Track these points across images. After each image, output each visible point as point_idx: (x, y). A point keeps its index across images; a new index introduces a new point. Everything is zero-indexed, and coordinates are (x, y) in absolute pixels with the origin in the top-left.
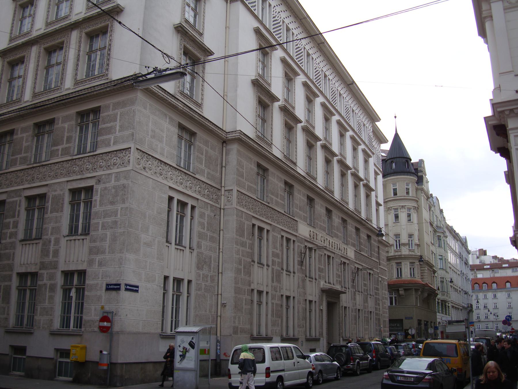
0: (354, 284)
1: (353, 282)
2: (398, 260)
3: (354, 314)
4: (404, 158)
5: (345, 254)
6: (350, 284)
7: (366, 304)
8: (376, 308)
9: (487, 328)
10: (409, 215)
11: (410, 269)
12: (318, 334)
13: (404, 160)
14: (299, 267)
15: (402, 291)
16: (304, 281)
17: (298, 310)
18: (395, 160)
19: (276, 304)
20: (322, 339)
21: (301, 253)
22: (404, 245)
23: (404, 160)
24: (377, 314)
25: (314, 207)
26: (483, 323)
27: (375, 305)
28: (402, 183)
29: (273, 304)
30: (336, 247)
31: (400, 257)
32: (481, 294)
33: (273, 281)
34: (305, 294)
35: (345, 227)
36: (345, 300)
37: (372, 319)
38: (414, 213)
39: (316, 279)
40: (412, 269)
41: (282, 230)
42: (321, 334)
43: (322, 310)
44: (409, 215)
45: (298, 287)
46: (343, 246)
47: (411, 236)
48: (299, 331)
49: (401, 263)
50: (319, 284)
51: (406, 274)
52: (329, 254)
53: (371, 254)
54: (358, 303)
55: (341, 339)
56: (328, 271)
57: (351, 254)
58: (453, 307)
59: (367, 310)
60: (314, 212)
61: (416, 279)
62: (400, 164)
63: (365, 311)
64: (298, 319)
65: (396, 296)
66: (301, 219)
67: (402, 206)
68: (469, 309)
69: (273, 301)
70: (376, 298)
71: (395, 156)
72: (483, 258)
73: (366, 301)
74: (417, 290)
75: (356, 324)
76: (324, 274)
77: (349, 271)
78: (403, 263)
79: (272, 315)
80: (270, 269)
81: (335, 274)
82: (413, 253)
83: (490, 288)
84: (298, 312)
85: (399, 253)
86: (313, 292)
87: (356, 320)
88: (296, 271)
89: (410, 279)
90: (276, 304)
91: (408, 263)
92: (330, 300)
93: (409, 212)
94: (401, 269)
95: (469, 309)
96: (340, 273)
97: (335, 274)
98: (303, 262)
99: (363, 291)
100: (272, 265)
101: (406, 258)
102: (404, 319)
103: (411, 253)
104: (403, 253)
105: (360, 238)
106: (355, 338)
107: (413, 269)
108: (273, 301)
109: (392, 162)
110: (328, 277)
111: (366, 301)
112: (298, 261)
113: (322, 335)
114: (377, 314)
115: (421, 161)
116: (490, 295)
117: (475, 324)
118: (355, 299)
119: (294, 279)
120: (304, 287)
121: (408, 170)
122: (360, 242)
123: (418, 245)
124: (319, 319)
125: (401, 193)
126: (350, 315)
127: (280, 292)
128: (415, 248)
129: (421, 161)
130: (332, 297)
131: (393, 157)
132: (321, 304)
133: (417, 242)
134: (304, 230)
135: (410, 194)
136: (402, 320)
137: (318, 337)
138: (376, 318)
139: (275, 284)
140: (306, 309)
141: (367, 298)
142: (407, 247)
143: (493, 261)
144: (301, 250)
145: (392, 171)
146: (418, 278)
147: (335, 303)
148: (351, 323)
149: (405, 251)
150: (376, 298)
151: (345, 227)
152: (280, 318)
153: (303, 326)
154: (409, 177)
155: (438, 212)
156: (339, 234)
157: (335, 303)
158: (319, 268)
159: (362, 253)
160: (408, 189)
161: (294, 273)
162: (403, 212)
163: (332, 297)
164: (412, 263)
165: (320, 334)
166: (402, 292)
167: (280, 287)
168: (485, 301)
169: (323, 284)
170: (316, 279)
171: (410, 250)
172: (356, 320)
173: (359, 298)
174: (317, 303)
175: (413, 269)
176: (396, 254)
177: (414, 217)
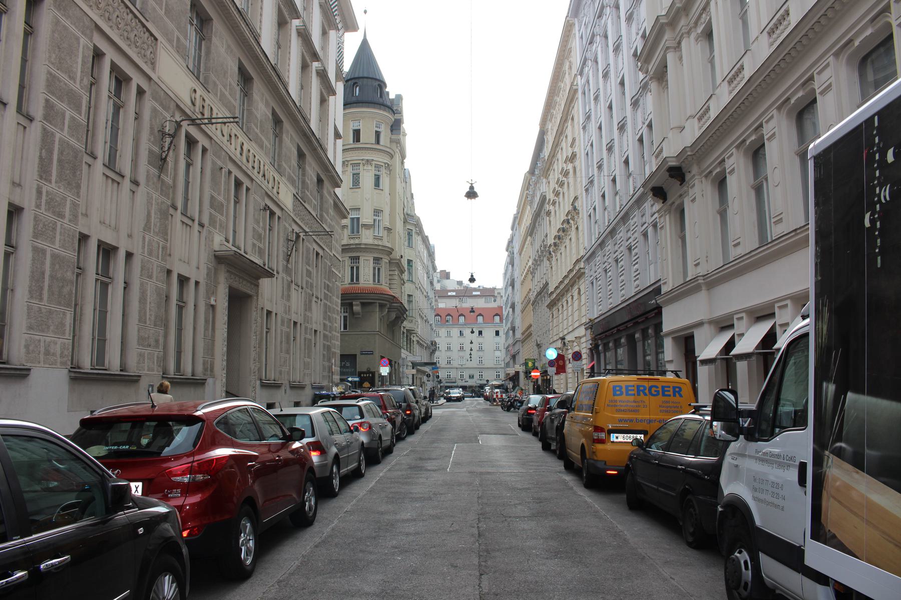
0: (289, 266)
1: (288, 261)
2: (354, 252)
3: (285, 329)
4: (376, 79)
5: (275, 191)
6: (282, 262)
7: (308, 314)
8: (325, 325)
9: (449, 376)
10: (377, 179)
11: (374, 268)
12: (200, 369)
13: (377, 83)
14: (154, 171)
15: (357, 305)
16: (165, 215)
17: (143, 293)
18: (360, 82)
19: (54, 256)
20: (210, 381)
21: (163, 134)
22: (367, 226)
23: (377, 83)
24: (325, 336)
25: (210, 40)
26: (444, 370)
27: (324, 319)
28: (369, 121)
29: (38, 252)
30: (256, 165)
31: (359, 248)
32: (443, 330)
33: (44, 172)
34: (167, 253)
35: (278, 135)
36: (269, 292)
37: (318, 344)
38: (385, 175)
39: (201, 225)
40: (377, 273)
41: (98, 27)
42: (209, 369)
43: (213, 306)
44: (377, 179)
45: (147, 228)
46: (271, 173)
47: (377, 212)
48: (141, 355)
49: (358, 258)
50: (210, 239)
51: (366, 279)
52: (241, 177)
53: (322, 216)
54: (293, 309)
55: (258, 382)
56: (235, 217)
57: (286, 197)
58: (418, 342)
59: (309, 326)
60: (208, 52)
61: (382, 287)
62: (366, 87)
63: (306, 328)
64: (142, 319)
65: (346, 314)
66: (170, 41)
67: (368, 160)
68: (433, 347)
69: (41, 244)
70: (325, 305)
71: (361, 75)
72: (446, 282)
73: (308, 307)
74: (382, 306)
75: (288, 352)
76: (223, 218)
77: (281, 234)
78: (361, 259)
79: (36, 291)
80: (35, 130)
81: (250, 229)
82: (380, 243)
83: (456, 323)
84: (143, 300)
85: (357, 241)
86: (191, 253)
87: (288, 342)
88: (142, 179)
89: (372, 286)
90: (54, 256)
91: (372, 259)
92: (236, 285)
93: (377, 173)
94: (358, 268)
95: (433, 348)
96: (260, 230)
97: (250, 229)
98: (164, 160)
99: (304, 286)
100: (47, 117)
101: (367, 249)
102: (358, 354)
103: (376, 242)
104: (364, 241)
105: (304, 175)
106: (286, 382)
107: (379, 269)
108: (41, 244)
109: (354, 84)
110: (235, 232)
111: (308, 307)
112: (151, 152)
113: (212, 370)
114: (325, 336)
115: (399, 98)
116: (455, 332)
117: (668, 373)
118: (289, 298)
119: (133, 200)
120: (164, 233)
121: (381, 100)
122: (304, 182)
123: (389, 230)
124: (206, 329)
125: (367, 137)
126: (279, 331)
127: (74, 218)
128: (383, 233)
129: (399, 98)
130: (241, 276)
131: (356, 76)
132: (212, 291)
133: (388, 224)
134: (174, 75)
135: (382, 142)
136: (355, 355)
137: (199, 375)
138: (324, 345)
139: (53, 187)
140: (167, 297)
141: (310, 301)
142: (372, 230)
143: (457, 287)
144: (163, 127)
145: (354, 99)
146: (384, 287)
147: (249, 297)
148: (279, 348)
149: (367, 237)
150: (325, 305)
151: (278, 135)
152: (68, 305)
153: (157, 341)
154: (381, 112)
155: (409, 196)
156: (266, 143)
157: (249, 297)
158: (212, 197)
159: (306, 205)
160: (378, 134)
161: (135, 183)
162: (368, 171)
163: (241, 276)
164: (377, 260)
165: (205, 370)
166: (357, 308)
167: (75, 206)
168: (449, 340)
169: (218, 240)
170: (201, 225)
171: (375, 238)
172: (288, 342)
173: (297, 299)
174: (202, 288)
175: (379, 269)
176: (352, 242)
177: (385, 181)
